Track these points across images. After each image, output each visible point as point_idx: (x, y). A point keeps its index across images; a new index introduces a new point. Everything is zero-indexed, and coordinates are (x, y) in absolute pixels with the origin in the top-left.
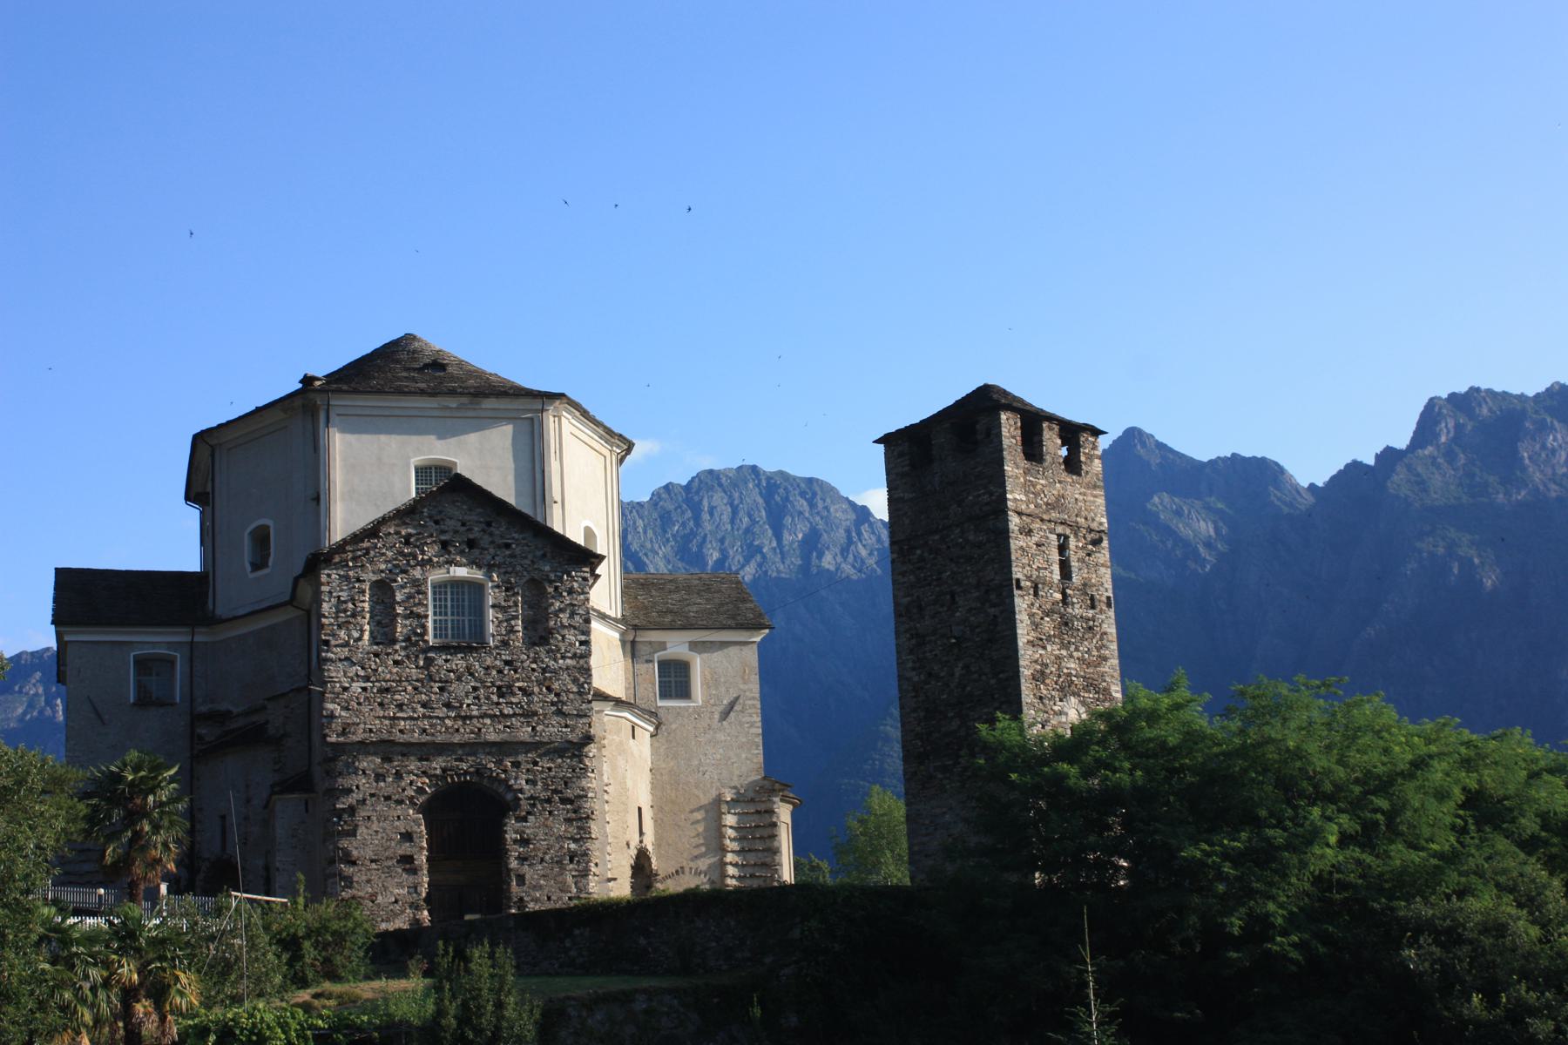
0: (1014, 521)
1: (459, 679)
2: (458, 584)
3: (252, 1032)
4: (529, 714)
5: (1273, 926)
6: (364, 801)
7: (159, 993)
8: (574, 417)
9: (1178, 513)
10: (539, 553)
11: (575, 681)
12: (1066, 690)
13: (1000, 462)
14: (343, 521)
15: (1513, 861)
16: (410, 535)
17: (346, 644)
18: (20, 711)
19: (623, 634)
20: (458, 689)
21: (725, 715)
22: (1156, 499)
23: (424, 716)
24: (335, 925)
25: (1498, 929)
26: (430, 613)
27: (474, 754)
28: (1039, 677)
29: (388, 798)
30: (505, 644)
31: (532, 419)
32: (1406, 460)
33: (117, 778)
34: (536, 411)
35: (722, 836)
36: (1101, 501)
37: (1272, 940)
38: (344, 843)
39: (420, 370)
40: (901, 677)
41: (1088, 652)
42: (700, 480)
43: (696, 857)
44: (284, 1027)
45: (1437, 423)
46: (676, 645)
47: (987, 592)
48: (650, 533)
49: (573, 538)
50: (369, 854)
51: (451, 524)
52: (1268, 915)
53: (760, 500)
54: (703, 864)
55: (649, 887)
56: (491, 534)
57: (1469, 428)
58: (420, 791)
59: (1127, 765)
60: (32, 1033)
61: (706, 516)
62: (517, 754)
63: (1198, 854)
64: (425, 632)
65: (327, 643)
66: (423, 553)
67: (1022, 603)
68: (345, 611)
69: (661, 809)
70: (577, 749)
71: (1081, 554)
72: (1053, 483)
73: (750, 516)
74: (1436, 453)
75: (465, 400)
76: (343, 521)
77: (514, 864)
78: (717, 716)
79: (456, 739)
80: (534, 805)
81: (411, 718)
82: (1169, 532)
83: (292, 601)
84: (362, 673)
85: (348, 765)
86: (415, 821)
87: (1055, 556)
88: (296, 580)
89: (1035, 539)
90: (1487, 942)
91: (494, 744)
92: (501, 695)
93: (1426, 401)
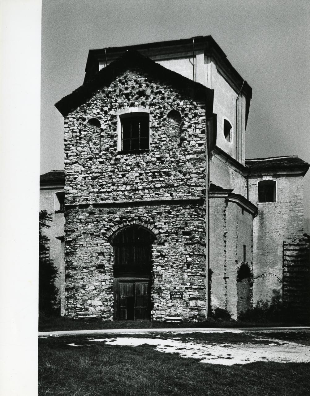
29: (92, 234)
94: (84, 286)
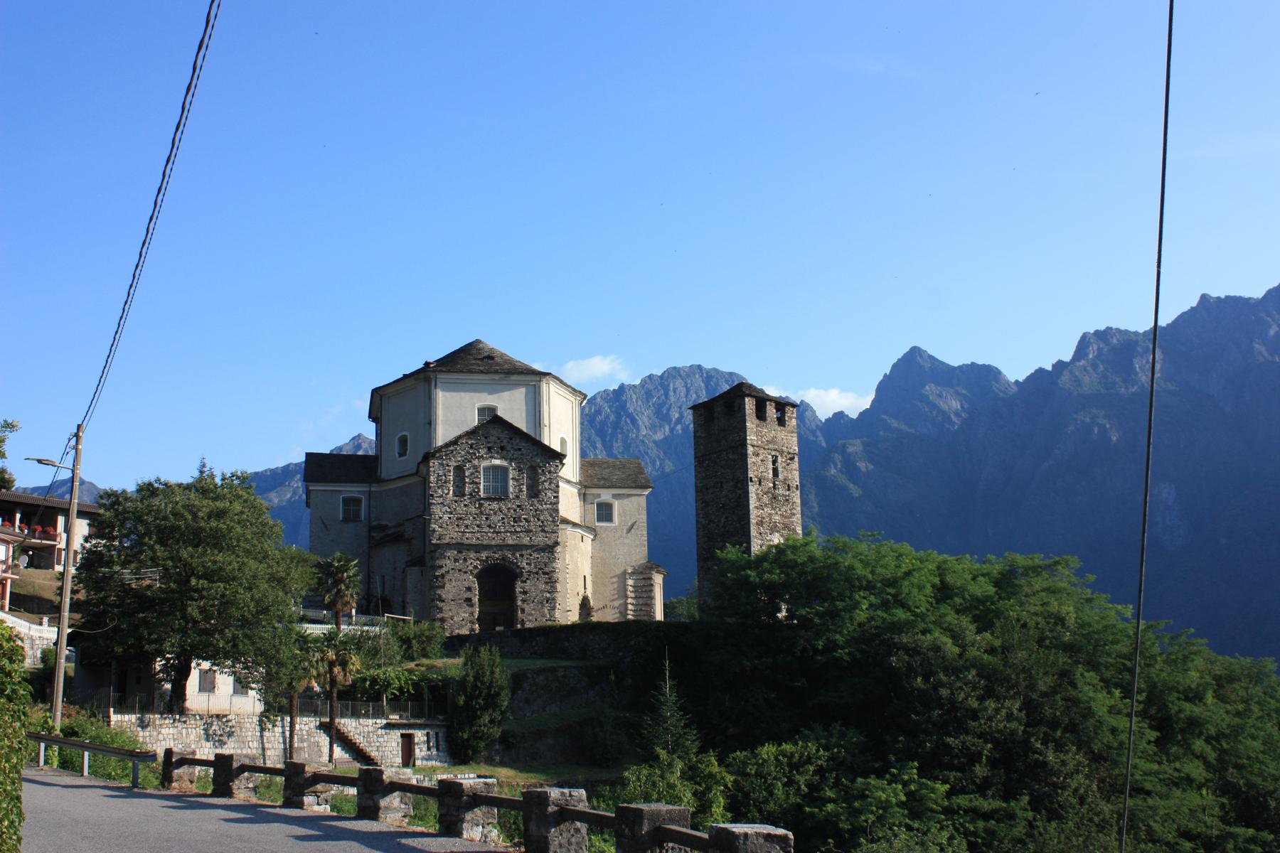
0: (750, 450)
1: (495, 514)
2: (495, 467)
3: (385, 681)
4: (528, 531)
5: (838, 645)
6: (448, 572)
7: (344, 664)
8: (556, 384)
9: (940, 396)
10: (535, 453)
11: (551, 515)
12: (773, 529)
13: (744, 421)
14: (442, 435)
15: (951, 617)
16: (472, 444)
17: (441, 496)
18: (289, 496)
19: (579, 490)
20: (494, 518)
21: (629, 530)
22: (927, 388)
23: (478, 532)
24: (427, 633)
25: (937, 648)
26: (482, 482)
27: (502, 550)
28: (760, 523)
29: (460, 570)
30: (517, 497)
31: (535, 385)
32: (1069, 368)
33: (331, 565)
34: (537, 381)
35: (626, 590)
36: (795, 439)
37: (836, 652)
38: (439, 592)
39: (482, 359)
40: (697, 521)
41: (786, 511)
42: (669, 373)
43: (613, 600)
44: (399, 679)
45: (1088, 347)
46: (606, 495)
47: (737, 483)
48: (640, 403)
49: (553, 447)
50: (451, 597)
51: (493, 438)
52: (836, 640)
53: (703, 385)
54: (617, 603)
55: (589, 614)
56: (512, 444)
57: (1106, 350)
58: (476, 567)
59: (778, 571)
60: (292, 679)
61: (671, 393)
62: (522, 550)
63: (804, 613)
64: (479, 491)
65: (432, 495)
66: (479, 452)
67: (753, 489)
68: (441, 480)
69: (596, 576)
70: (550, 549)
71: (784, 464)
72: (771, 430)
73: (696, 393)
74: (1086, 364)
75: (502, 376)
76: (442, 435)
77: (519, 603)
78: (625, 531)
79: (493, 543)
80: (529, 575)
81: (472, 532)
82: (935, 406)
83: (417, 473)
84: (449, 510)
85: (441, 554)
86: (473, 582)
87: (771, 466)
88: (419, 464)
89: (761, 458)
90: (931, 654)
91: (511, 545)
92: (515, 522)
93: (1081, 335)
94: (453, 616)
